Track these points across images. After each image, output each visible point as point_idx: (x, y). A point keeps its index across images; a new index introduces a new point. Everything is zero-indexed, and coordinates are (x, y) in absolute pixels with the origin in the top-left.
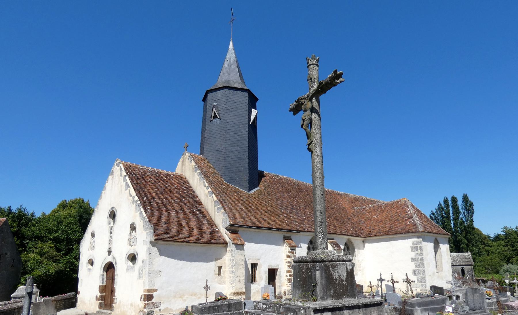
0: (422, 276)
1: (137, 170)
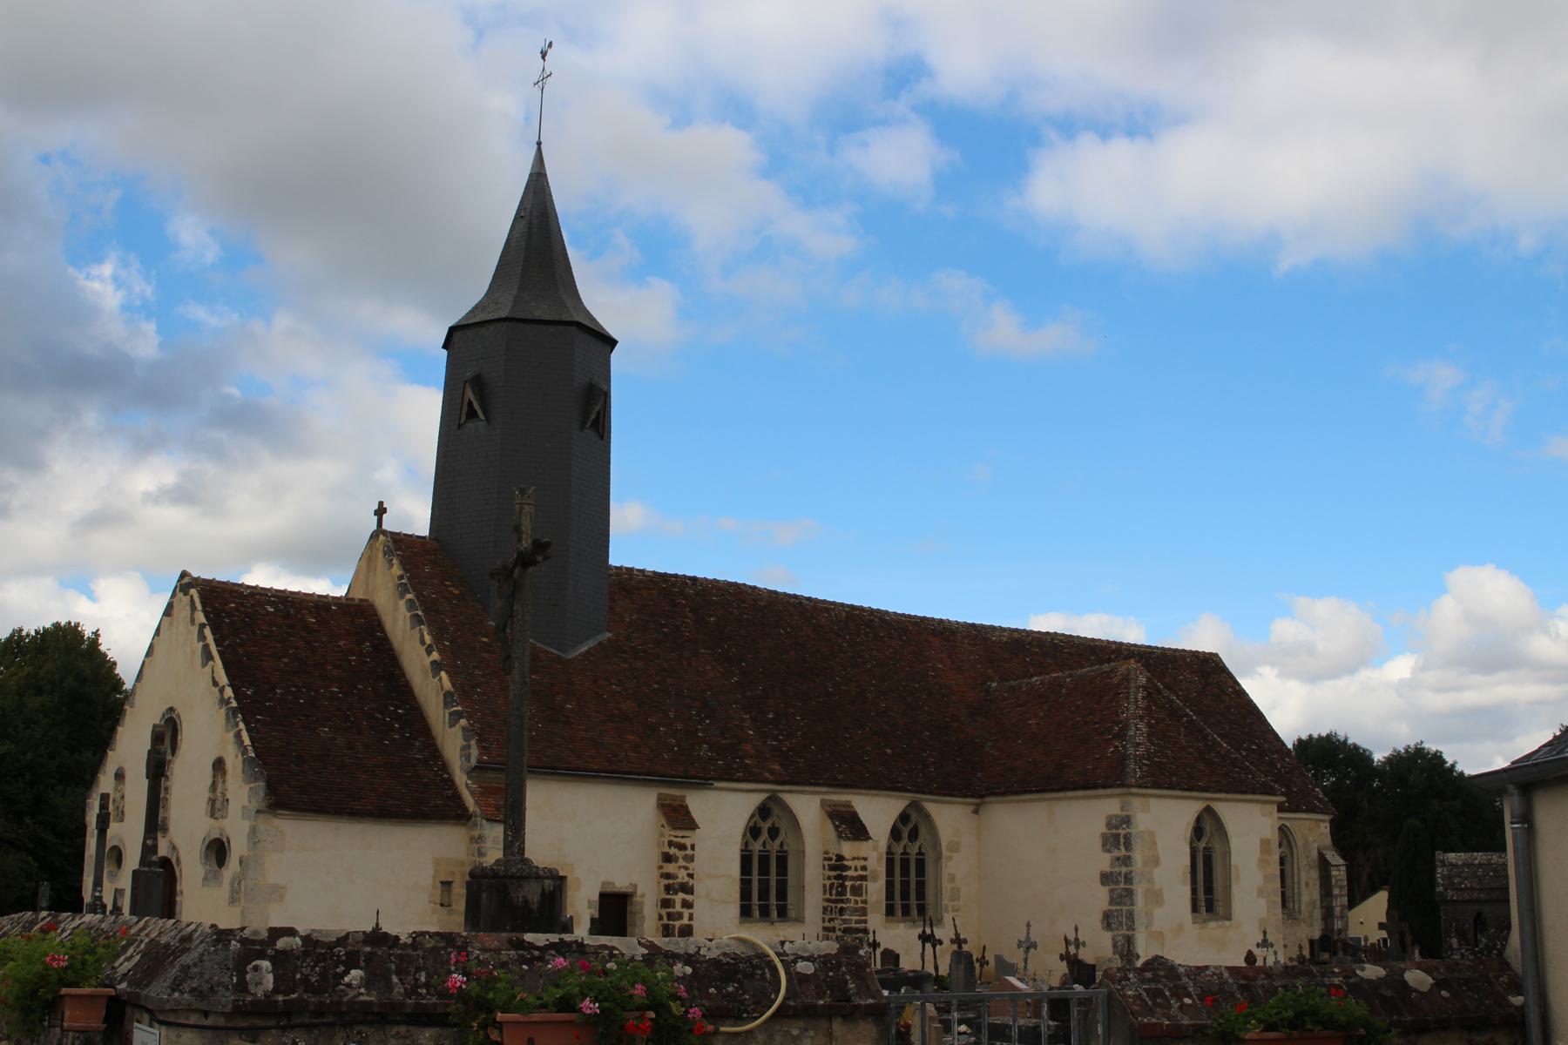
0: (1127, 933)
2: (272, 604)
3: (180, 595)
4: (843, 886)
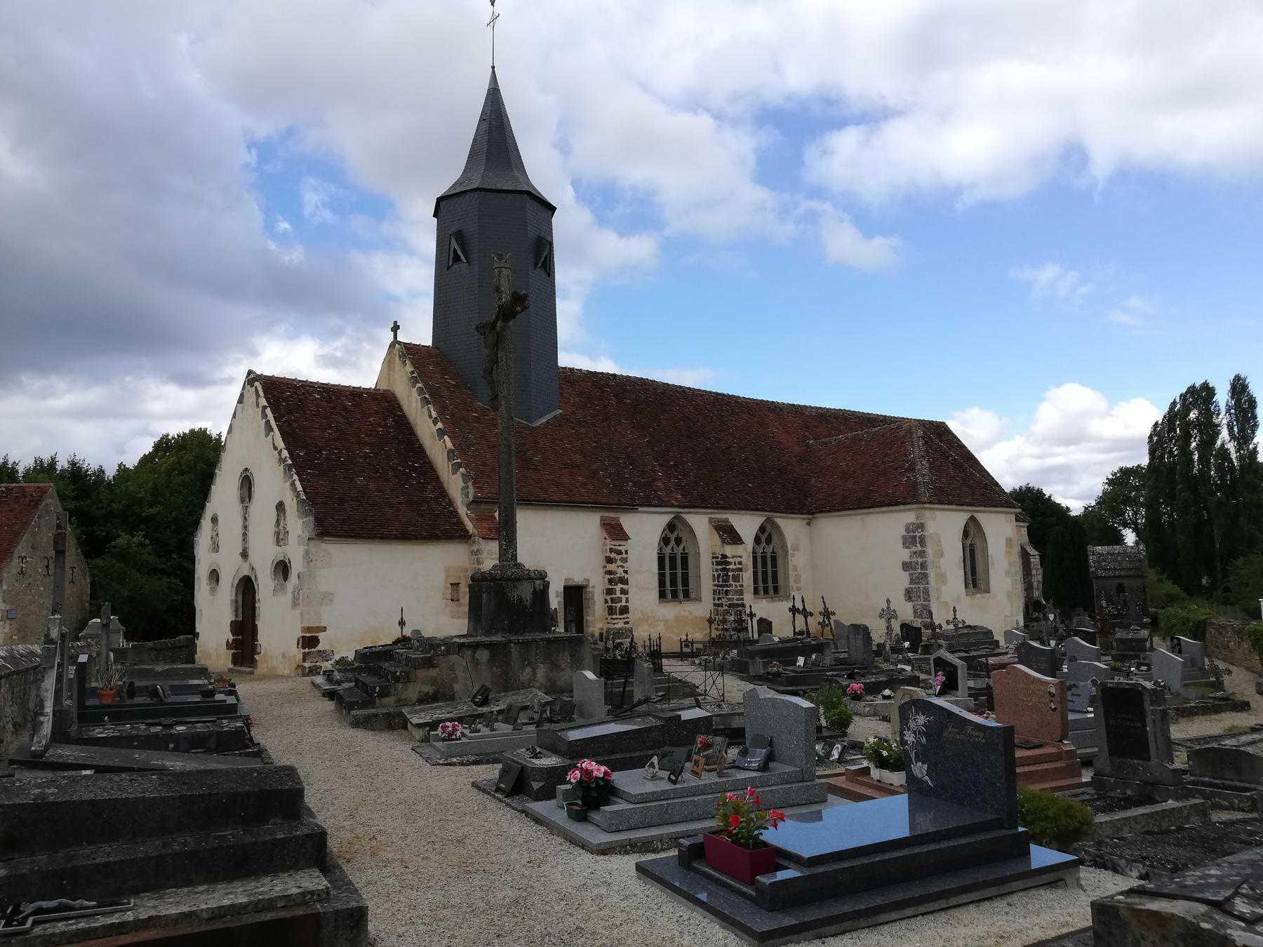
1: (289, 392)
2: (319, 393)
3: (248, 387)
4: (727, 575)
